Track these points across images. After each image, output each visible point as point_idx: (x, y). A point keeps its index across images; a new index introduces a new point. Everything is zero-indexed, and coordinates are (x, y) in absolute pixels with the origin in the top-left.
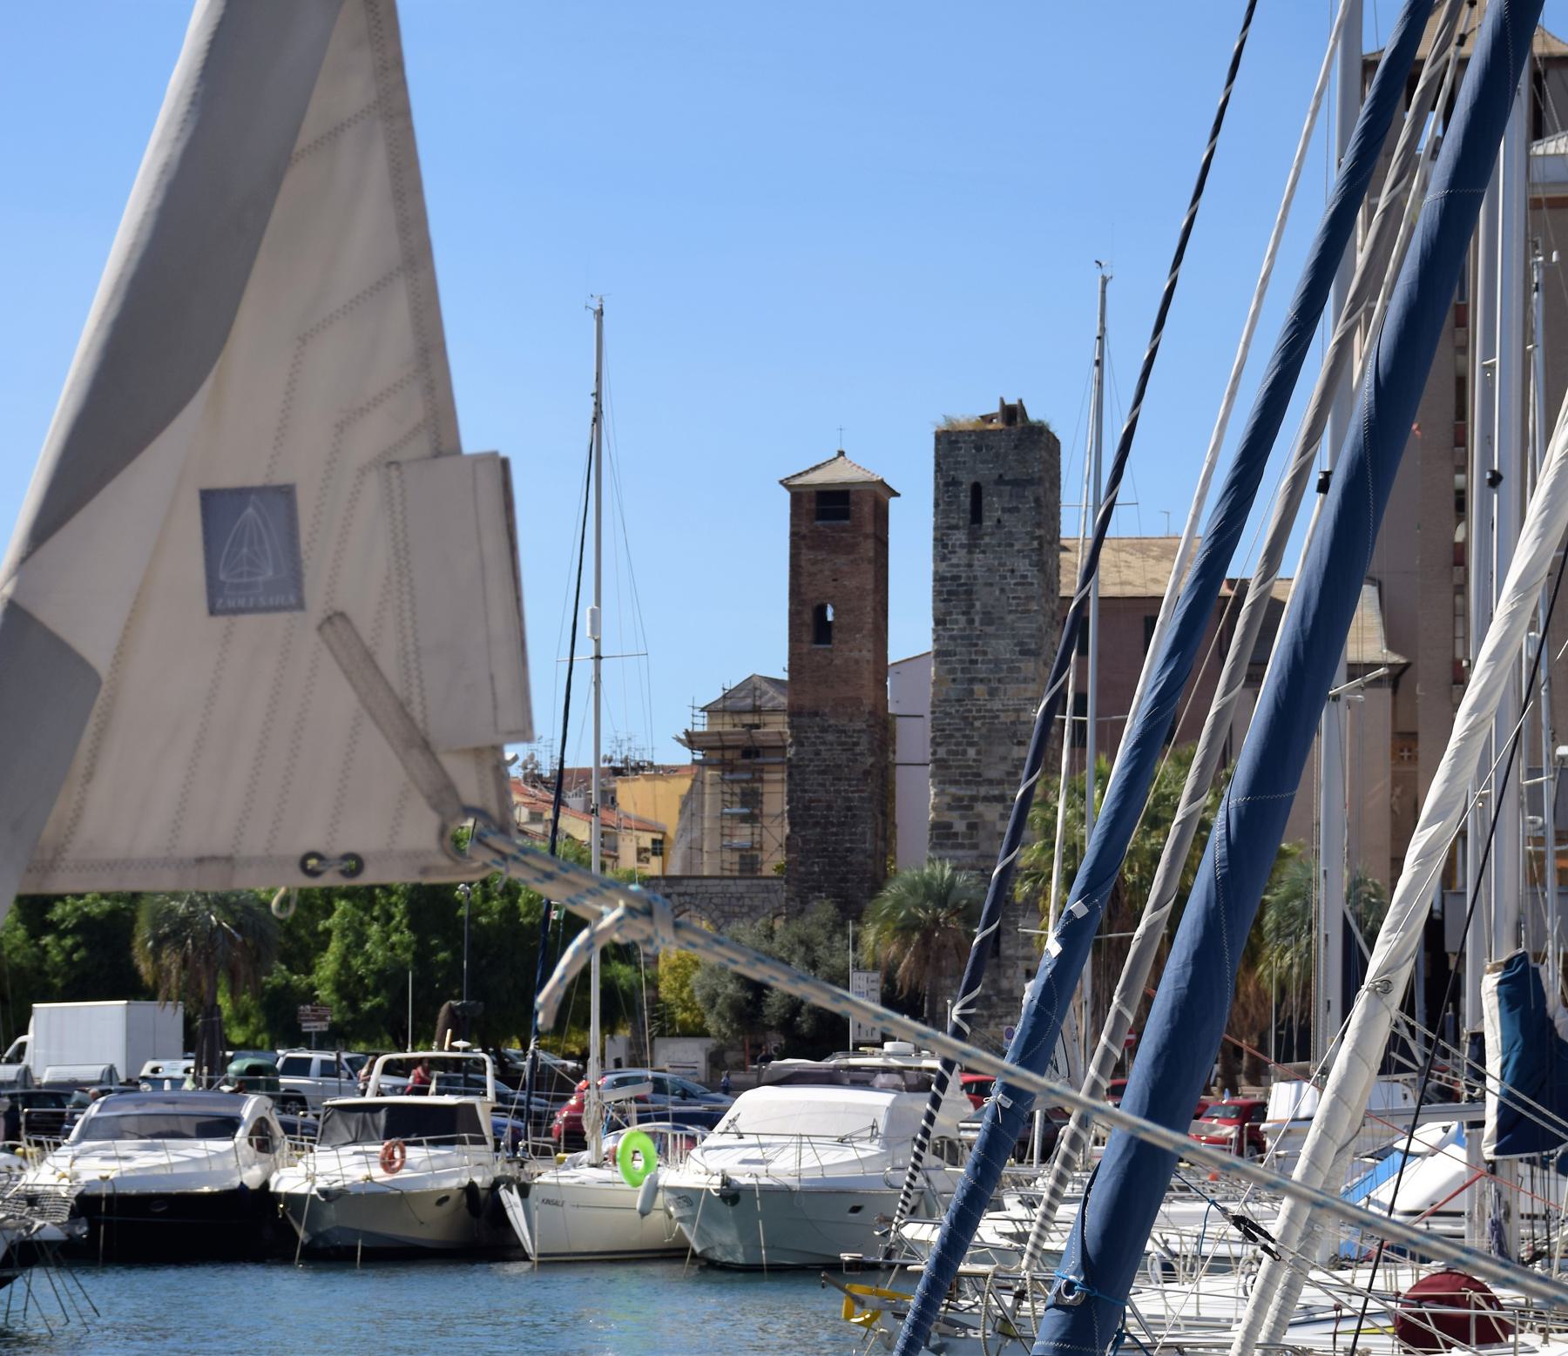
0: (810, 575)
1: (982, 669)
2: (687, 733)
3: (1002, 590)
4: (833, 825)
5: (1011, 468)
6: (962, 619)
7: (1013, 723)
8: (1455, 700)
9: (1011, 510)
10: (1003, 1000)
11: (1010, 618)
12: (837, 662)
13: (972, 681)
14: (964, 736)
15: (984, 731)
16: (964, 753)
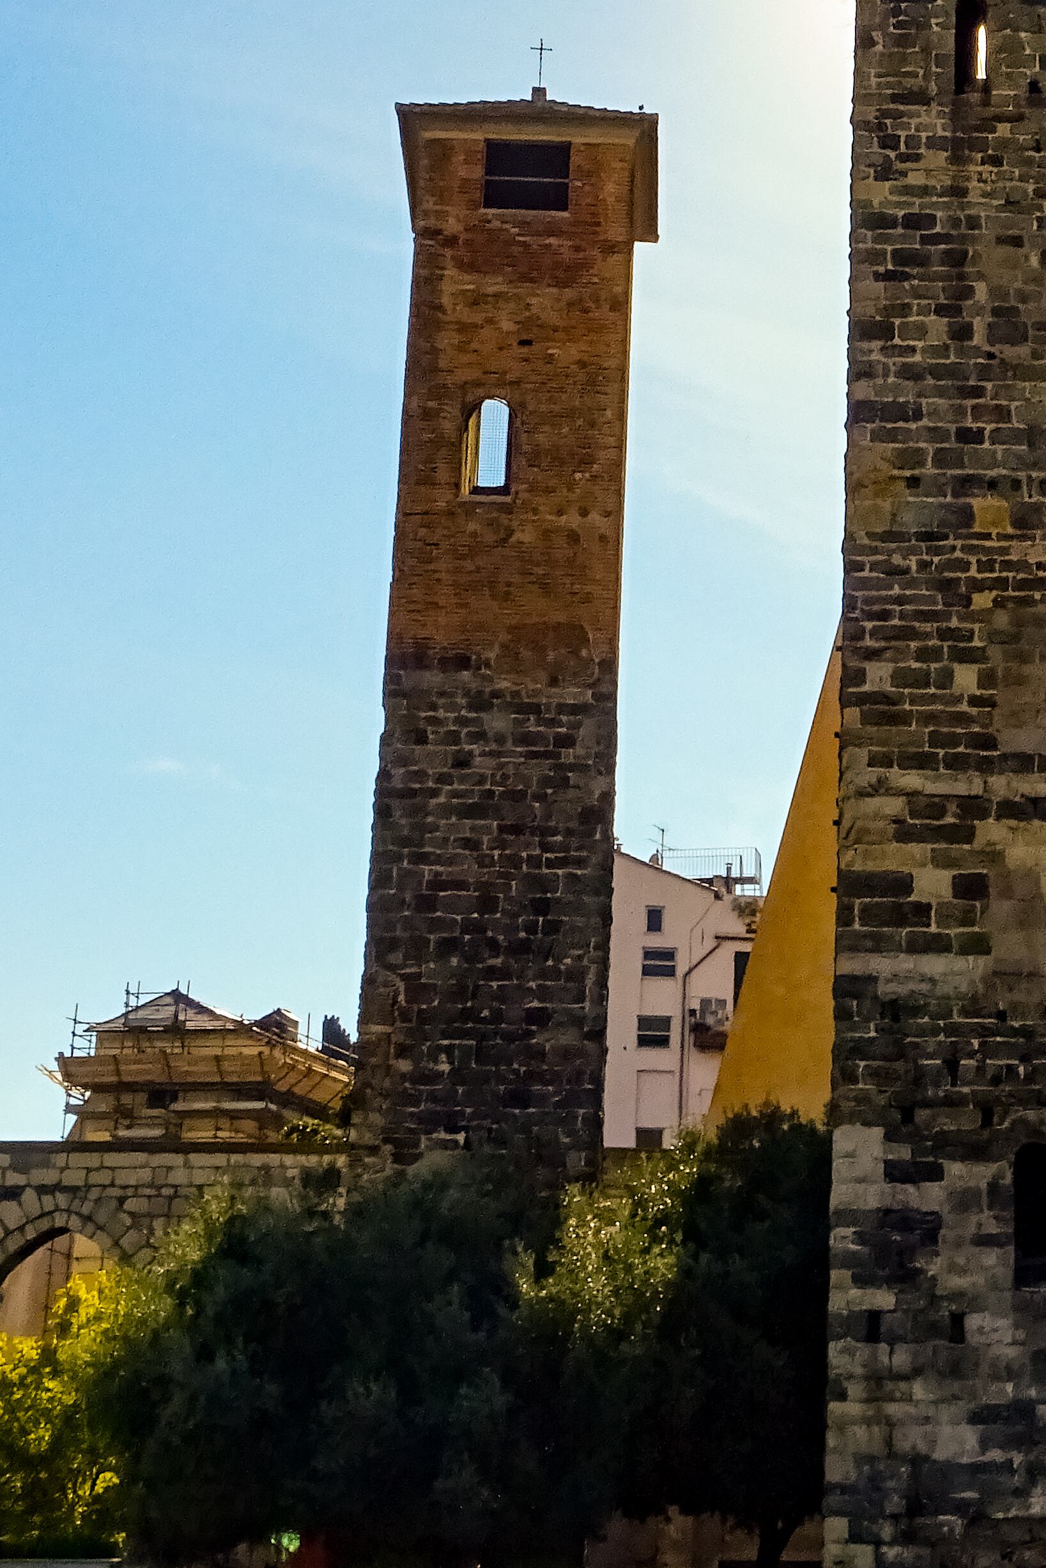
0: (463, 328)
2: (61, 1058)
4: (493, 946)
6: (938, 326)
12: (525, 536)
13: (965, 485)
14: (944, 634)
15: (1002, 620)
16: (947, 678)
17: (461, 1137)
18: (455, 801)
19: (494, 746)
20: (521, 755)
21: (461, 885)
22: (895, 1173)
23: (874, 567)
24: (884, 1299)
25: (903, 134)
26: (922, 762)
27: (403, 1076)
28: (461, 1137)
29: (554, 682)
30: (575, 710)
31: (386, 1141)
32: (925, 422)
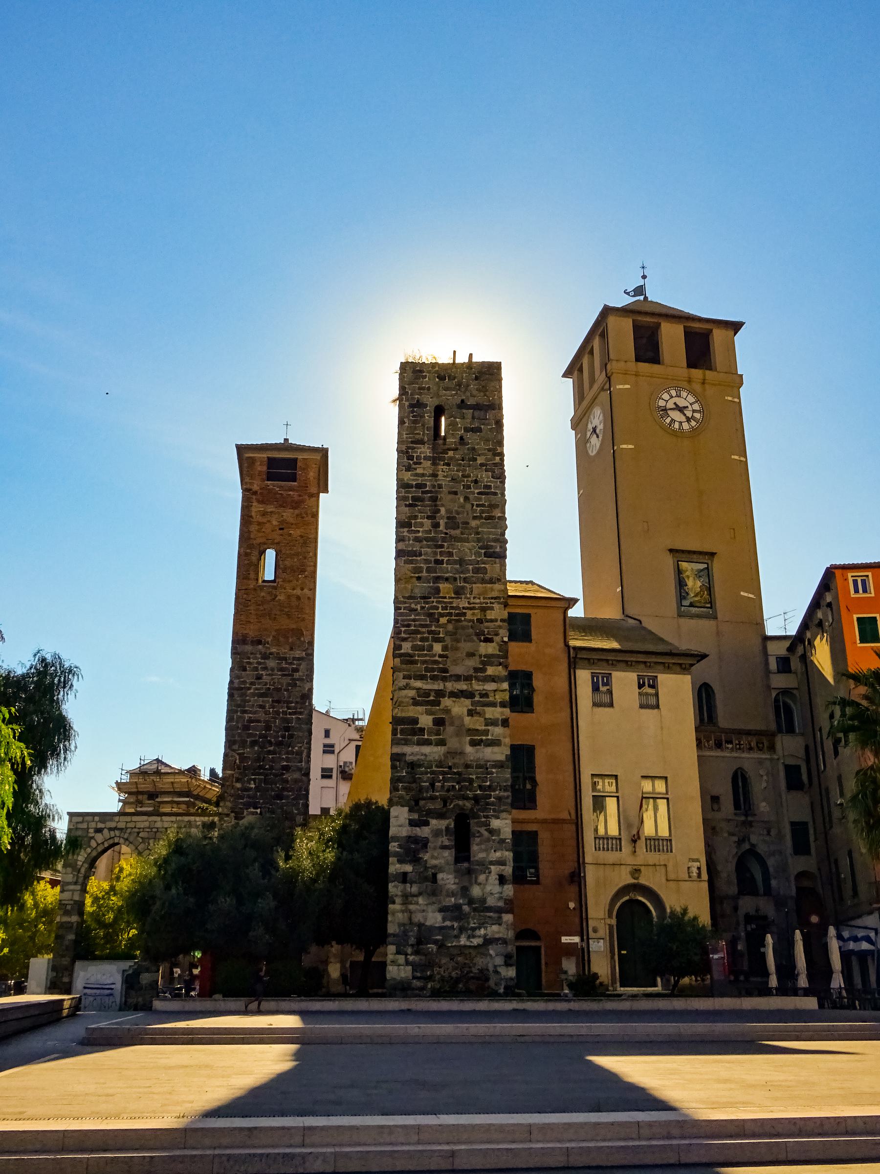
0: (259, 524)
1: (448, 569)
2: (117, 783)
3: (466, 499)
4: (270, 743)
5: (472, 396)
6: (427, 523)
7: (480, 621)
9: (473, 430)
10: (475, 910)
11: (474, 523)
13: (437, 579)
14: (430, 632)
15: (450, 627)
16: (431, 648)
17: (259, 811)
21: (258, 721)
22: (412, 823)
24: (408, 868)
25: (415, 455)
26: (422, 678)
27: (238, 789)
28: (259, 811)
29: (291, 649)
30: (299, 659)
31: (232, 812)
32: (423, 557)
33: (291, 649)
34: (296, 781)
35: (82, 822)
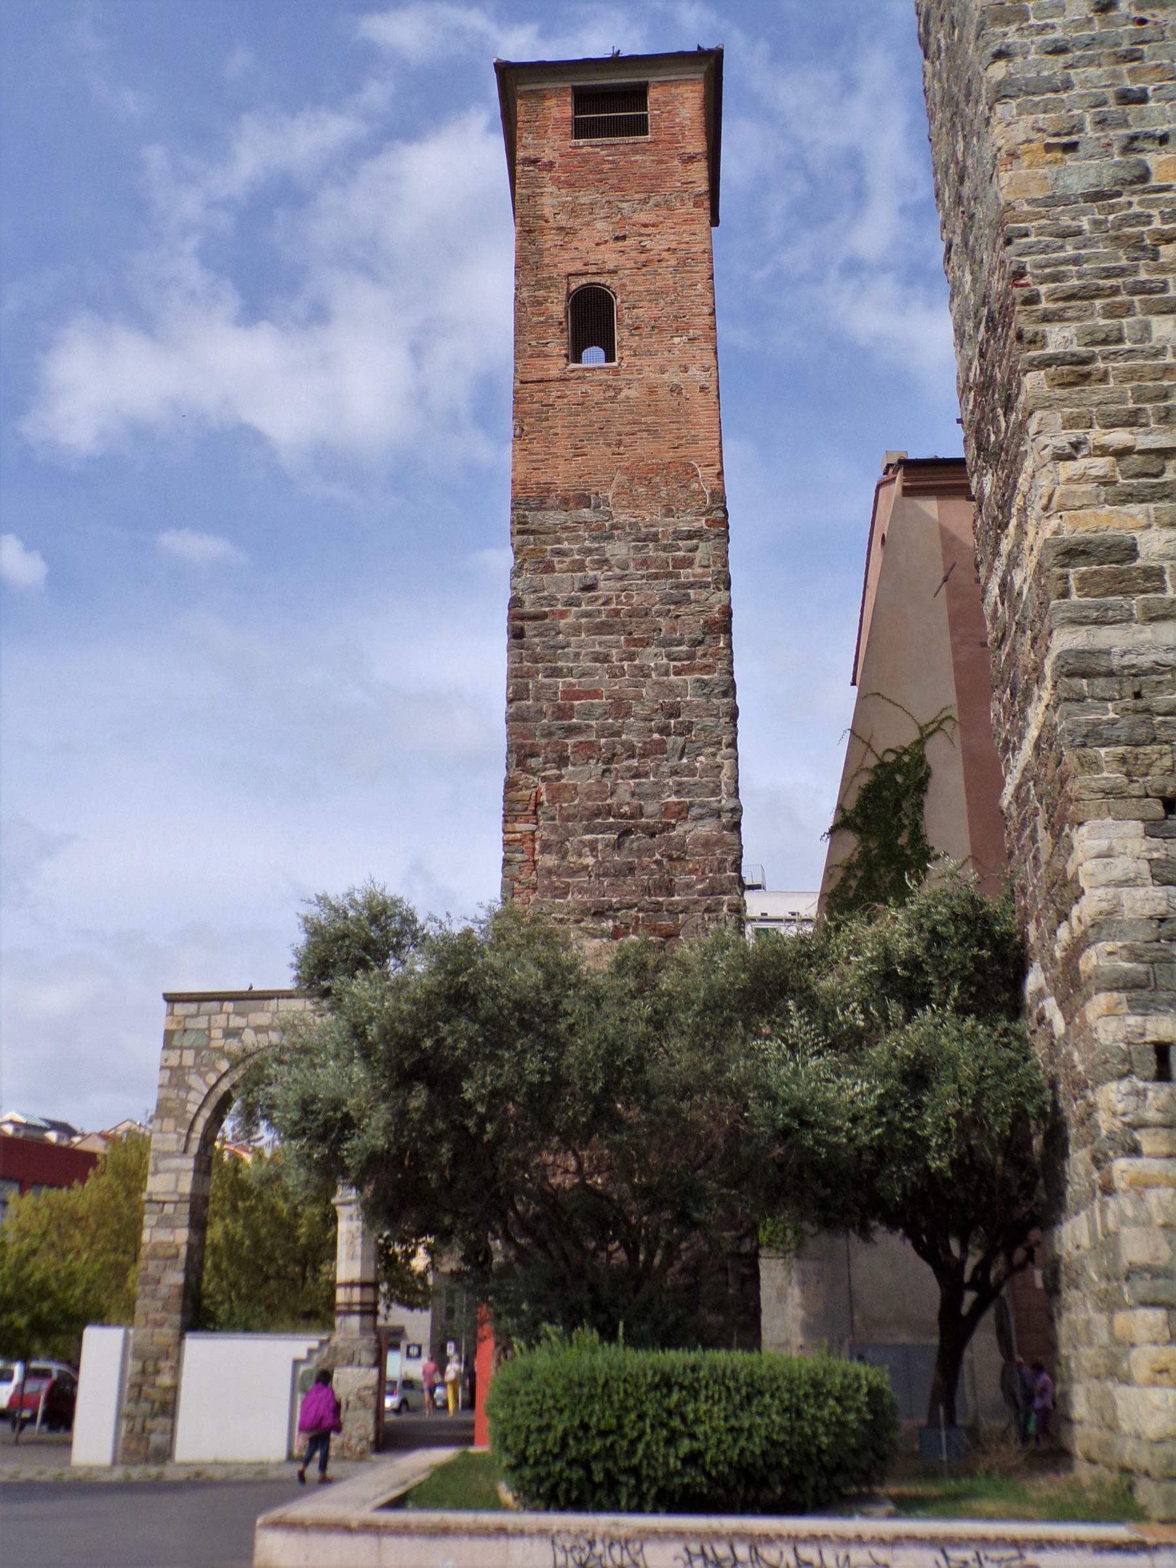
8: (256, 1322)
18: (583, 620)
19: (617, 571)
20: (643, 577)
23: (1041, 231)
26: (1132, 420)
27: (550, 872)
29: (669, 513)
30: (690, 536)
33: (669, 513)
34: (707, 844)
35: (197, 1015)
